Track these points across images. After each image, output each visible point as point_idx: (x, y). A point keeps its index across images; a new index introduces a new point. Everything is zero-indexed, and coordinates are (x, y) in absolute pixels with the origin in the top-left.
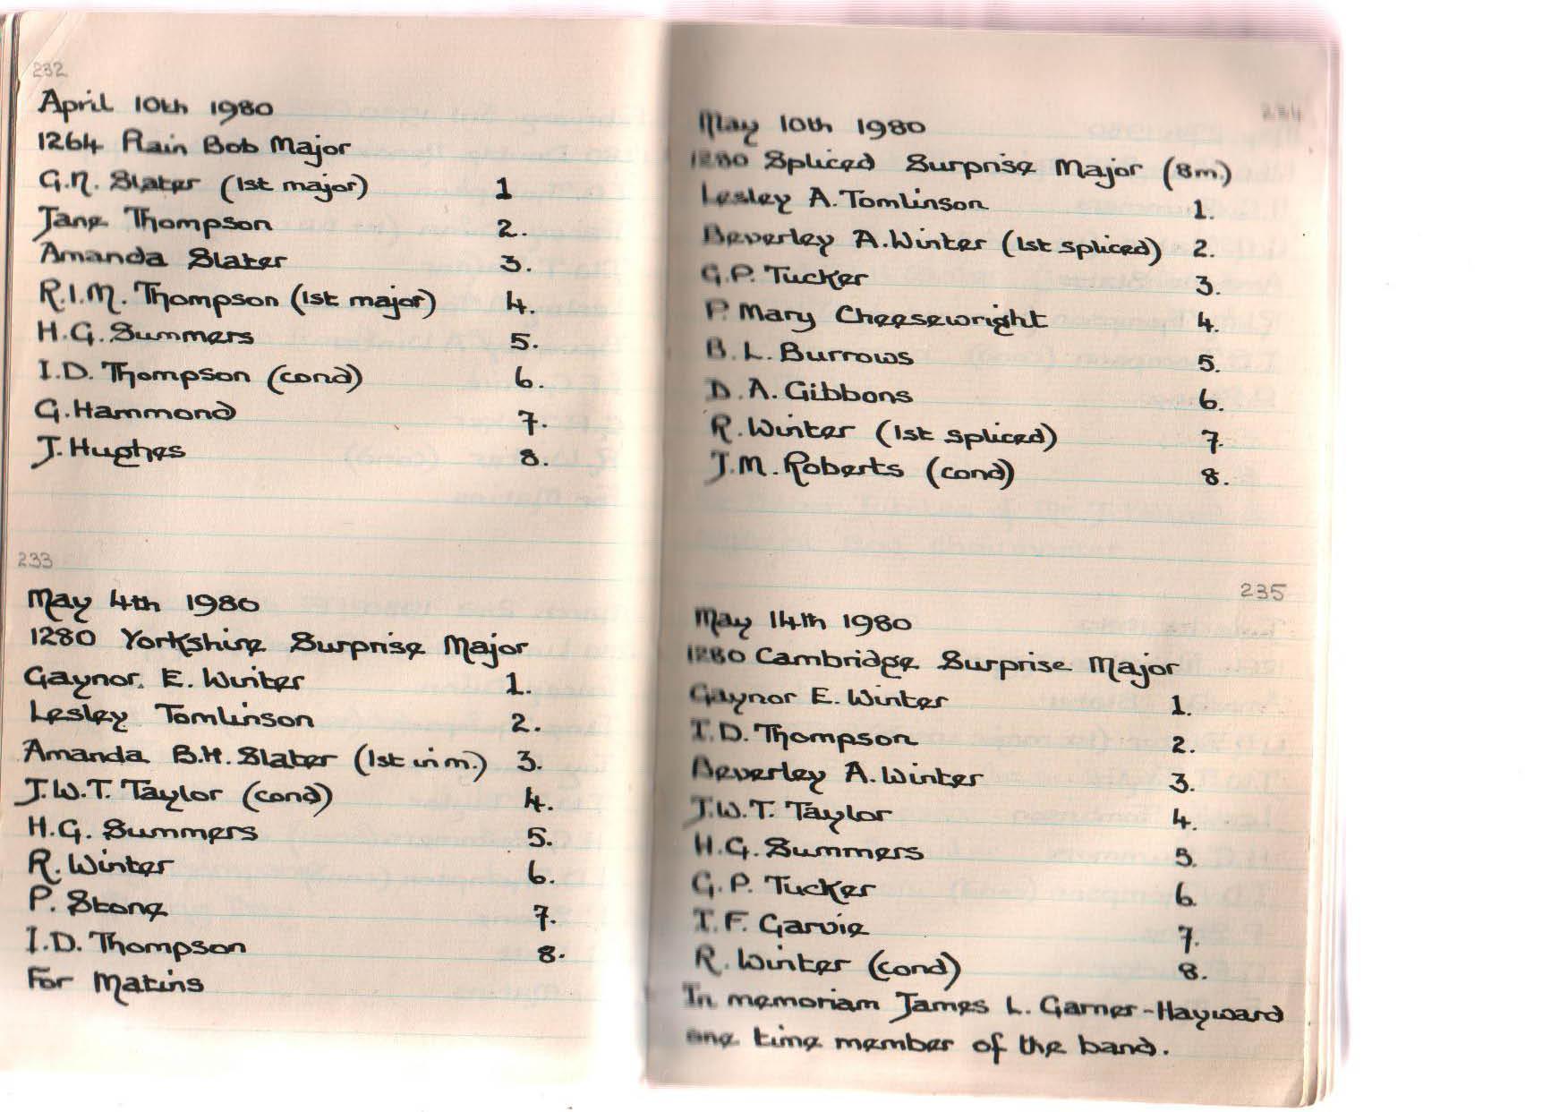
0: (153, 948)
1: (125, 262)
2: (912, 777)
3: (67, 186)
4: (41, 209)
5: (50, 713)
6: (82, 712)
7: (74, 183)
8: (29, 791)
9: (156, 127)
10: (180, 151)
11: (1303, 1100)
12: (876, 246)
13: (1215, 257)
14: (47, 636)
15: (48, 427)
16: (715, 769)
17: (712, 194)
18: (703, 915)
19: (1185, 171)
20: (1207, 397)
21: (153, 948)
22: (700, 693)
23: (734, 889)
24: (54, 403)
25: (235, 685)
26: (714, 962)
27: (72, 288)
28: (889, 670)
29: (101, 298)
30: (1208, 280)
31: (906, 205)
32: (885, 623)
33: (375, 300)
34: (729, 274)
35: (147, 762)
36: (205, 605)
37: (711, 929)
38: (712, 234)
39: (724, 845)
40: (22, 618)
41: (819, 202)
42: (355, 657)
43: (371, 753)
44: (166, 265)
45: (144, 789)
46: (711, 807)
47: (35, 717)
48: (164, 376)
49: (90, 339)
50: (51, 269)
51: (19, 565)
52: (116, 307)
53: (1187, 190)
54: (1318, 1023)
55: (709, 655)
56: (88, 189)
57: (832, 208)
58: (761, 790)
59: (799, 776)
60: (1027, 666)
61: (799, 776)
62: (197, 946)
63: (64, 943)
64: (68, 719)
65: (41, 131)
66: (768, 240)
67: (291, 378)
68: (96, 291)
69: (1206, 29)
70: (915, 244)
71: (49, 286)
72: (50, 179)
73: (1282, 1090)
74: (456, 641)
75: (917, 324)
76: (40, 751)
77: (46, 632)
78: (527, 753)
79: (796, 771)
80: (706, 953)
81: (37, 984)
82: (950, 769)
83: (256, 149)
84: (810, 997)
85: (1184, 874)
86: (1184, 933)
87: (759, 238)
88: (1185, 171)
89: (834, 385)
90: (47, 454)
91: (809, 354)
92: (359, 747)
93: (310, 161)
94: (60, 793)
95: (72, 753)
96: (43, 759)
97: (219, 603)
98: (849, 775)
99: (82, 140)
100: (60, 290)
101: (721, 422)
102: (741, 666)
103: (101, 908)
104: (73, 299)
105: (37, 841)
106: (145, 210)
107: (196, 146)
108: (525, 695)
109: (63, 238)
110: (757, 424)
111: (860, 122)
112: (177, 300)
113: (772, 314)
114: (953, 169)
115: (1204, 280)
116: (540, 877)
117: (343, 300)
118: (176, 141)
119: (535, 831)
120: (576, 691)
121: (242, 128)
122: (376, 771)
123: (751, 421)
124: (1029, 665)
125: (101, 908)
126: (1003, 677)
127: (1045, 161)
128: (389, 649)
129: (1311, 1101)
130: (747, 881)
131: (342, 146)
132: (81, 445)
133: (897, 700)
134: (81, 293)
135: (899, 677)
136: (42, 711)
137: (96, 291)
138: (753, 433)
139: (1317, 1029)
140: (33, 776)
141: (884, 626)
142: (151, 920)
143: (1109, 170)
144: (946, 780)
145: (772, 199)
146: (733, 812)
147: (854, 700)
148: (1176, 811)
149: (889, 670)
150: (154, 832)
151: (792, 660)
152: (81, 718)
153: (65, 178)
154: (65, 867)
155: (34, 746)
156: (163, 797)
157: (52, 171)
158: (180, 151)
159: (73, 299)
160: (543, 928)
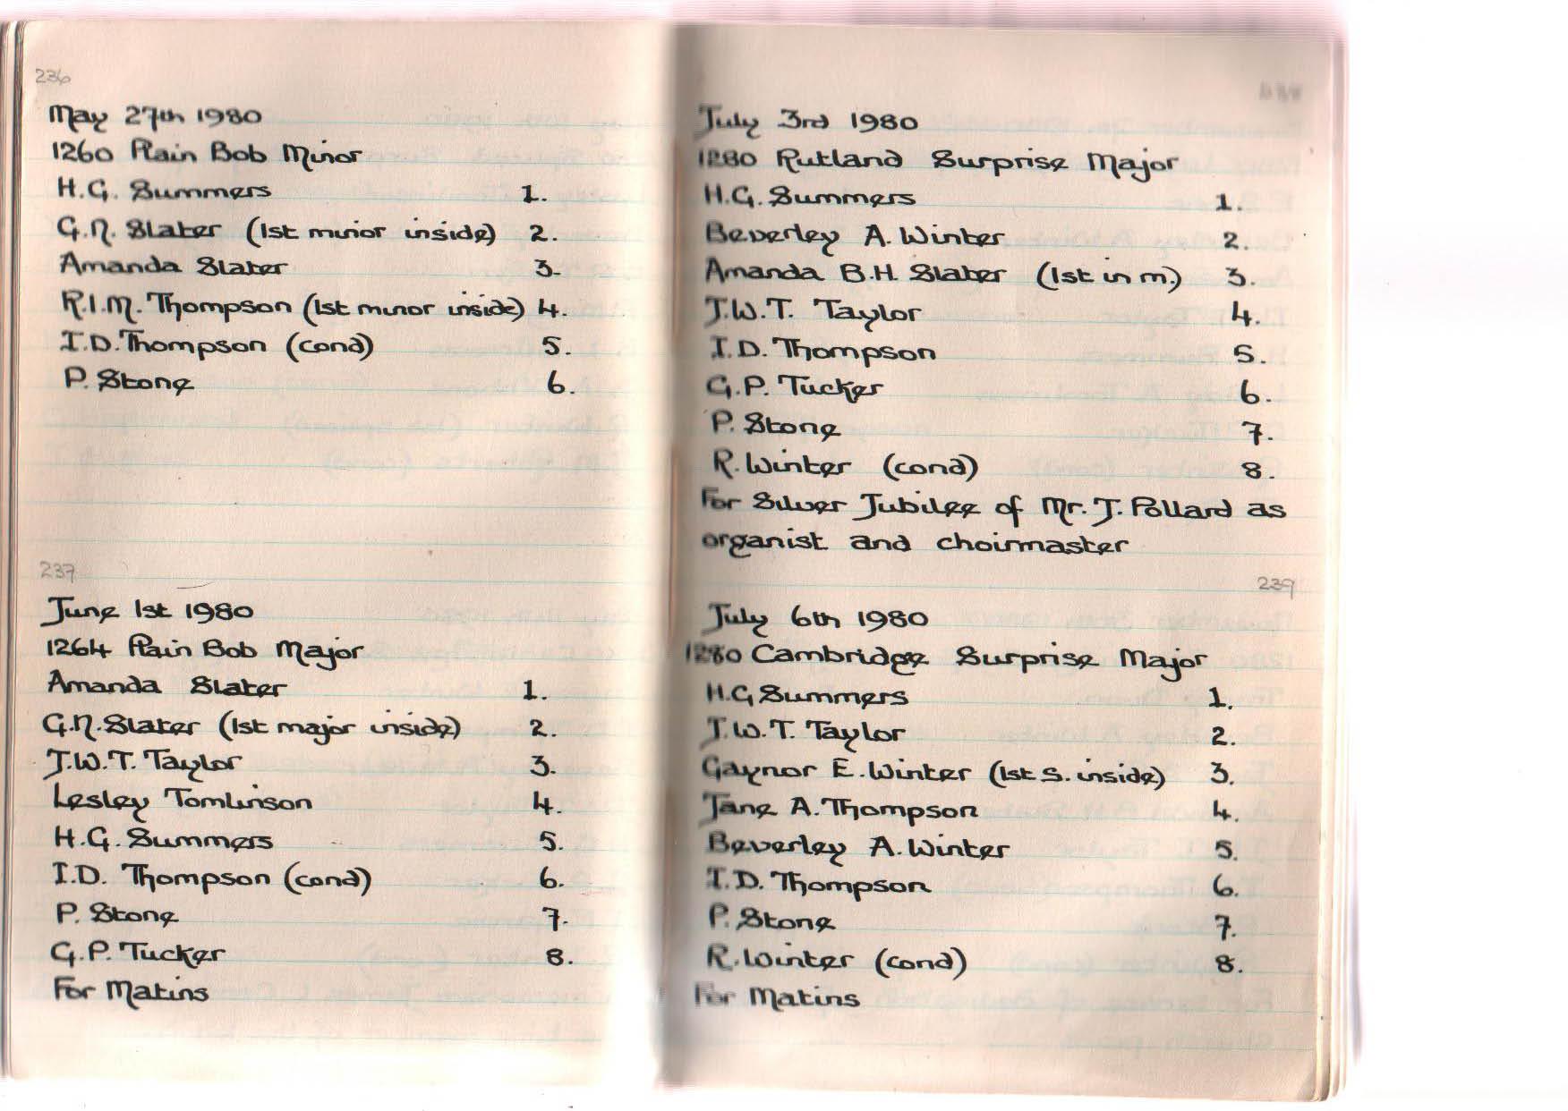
0: (176, 347)
1: (144, 271)
2: (934, 236)
3: (72, 729)
5: (70, 799)
6: (101, 799)
7: (94, 233)
10: (189, 158)
11: (1317, 1095)
14: (61, 648)
15: (55, 741)
16: (727, 233)
17: (63, 799)
18: (718, 609)
21: (176, 347)
22: (712, 767)
26: (725, 960)
27: (92, 298)
28: (900, 668)
32: (899, 619)
37: (723, 886)
38: (712, 159)
40: (31, 638)
41: (882, 852)
43: (263, 226)
46: (726, 308)
47: (57, 804)
50: (71, 280)
51: (43, 576)
52: (134, 316)
54: (1330, 1018)
56: (93, 733)
57: (896, 856)
58: (776, 287)
59: (819, 849)
60: (1050, 660)
61: (819, 849)
62: (220, 345)
63: (89, 876)
64: (88, 805)
67: (306, 881)
68: (116, 303)
69: (1211, 27)
71: (75, 296)
73: (1297, 1082)
74: (1132, 654)
76: (75, 263)
77: (67, 149)
78: (541, 757)
79: (816, 845)
80: (717, 951)
81: (63, 993)
83: (264, 158)
85: (1225, 867)
86: (1222, 921)
90: (56, 769)
91: (797, 197)
93: (322, 664)
94: (81, 764)
95: (92, 686)
96: (79, 272)
97: (216, 611)
101: (723, 456)
102: (753, 169)
103: (129, 384)
104: (93, 309)
105: (69, 359)
106: (794, 341)
107: (204, 153)
109: (72, 668)
111: (854, 116)
114: (1009, 661)
116: (558, 385)
117: (353, 308)
118: (185, 148)
119: (547, 835)
120: (587, 697)
121: (236, 137)
124: (1052, 659)
125: (129, 384)
126: (1025, 670)
128: (1061, 660)
129: (1324, 1097)
131: (354, 651)
132: (98, 648)
133: (919, 773)
134: (101, 303)
135: (912, 674)
136: (63, 799)
137: (116, 303)
139: (1329, 1024)
141: (899, 622)
142: (178, 394)
144: (974, 852)
145: (827, 848)
147: (916, 851)
149: (900, 668)
151: (765, 273)
152: (100, 805)
153: (69, 723)
156: (184, 766)
157: (68, 217)
158: (189, 158)
159: (93, 309)
160: (555, 928)
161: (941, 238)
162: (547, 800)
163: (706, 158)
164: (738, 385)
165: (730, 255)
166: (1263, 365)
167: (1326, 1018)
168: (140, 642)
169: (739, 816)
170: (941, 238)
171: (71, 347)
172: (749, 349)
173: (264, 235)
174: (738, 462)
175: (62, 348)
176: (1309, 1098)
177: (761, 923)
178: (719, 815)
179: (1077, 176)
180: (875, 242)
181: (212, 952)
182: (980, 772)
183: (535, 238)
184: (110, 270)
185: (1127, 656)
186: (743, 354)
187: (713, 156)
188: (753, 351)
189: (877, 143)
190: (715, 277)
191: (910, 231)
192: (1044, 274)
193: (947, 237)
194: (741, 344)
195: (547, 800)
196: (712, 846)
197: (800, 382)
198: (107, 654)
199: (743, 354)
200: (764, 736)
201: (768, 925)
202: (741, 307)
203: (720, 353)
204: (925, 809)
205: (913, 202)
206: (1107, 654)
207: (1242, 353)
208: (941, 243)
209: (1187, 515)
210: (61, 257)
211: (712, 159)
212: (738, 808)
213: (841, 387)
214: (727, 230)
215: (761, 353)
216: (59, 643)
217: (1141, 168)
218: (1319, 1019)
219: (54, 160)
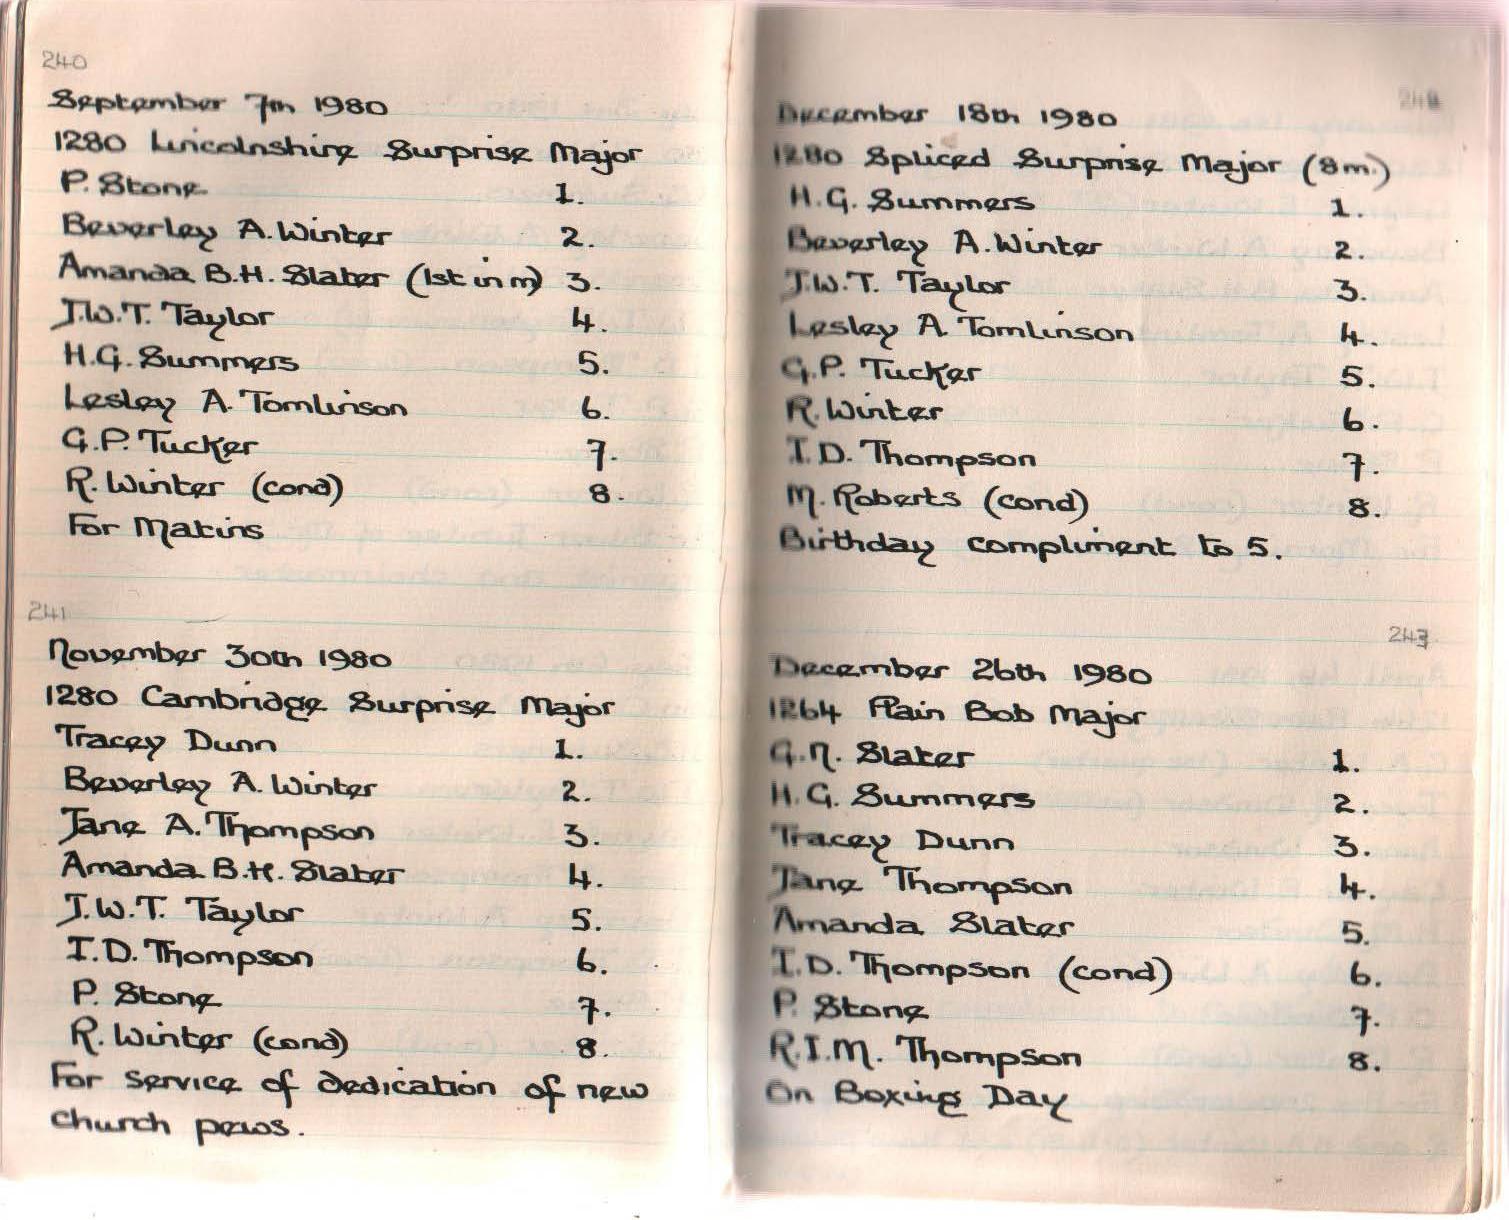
2: (1028, 244)
4: (58, 728)
7: (814, 755)
8: (62, 313)
9: (910, 692)
11: (1467, 1206)
12: (976, 250)
13: (1364, 217)
19: (1329, 166)
20: (1352, 418)
23: (824, 373)
24: (81, 432)
25: (143, 490)
29: (152, 533)
30: (1350, 285)
31: (1032, 334)
33: (108, 271)
34: (818, 371)
35: (193, 281)
36: (1092, 674)
37: (805, 460)
38: (789, 709)
39: (825, 197)
40: (35, 672)
42: (1089, 176)
43: (427, 272)
44: (65, 301)
45: (187, 312)
46: (807, 281)
47: (69, 405)
48: (203, 362)
49: (116, 364)
53: (1331, 186)
55: (75, 697)
58: (861, 261)
65: (49, 684)
66: (855, 246)
70: (1023, 247)
72: (74, 438)
73: (1446, 1193)
75: (1022, 208)
76: (75, 265)
81: (62, 1083)
82: (1072, 239)
83: (1031, 718)
84: (879, 1090)
87: (846, 243)
88: (1329, 166)
89: (813, 704)
92: (414, 266)
98: (960, 244)
99: (818, 708)
100: (96, 1031)
102: (840, 168)
108: (575, 760)
110: (836, 405)
112: (193, 958)
113: (836, 925)
115: (1345, 285)
122: (435, 291)
123: (829, 402)
127: (1168, 155)
129: (1475, 1208)
130: (839, 362)
136: (77, 397)
138: (831, 416)
140: (70, 296)
143: (1242, 164)
146: (831, 286)
148: (1345, 326)
150: (192, 360)
154: (103, 484)
155: (69, 259)
157: (76, 429)
161: (1036, 247)
162: (587, 317)
163: (778, 710)
164: (814, 367)
165: (803, 904)
166: (1374, 347)
167: (1478, 1120)
168: (887, 703)
169: (816, 893)
170: (1036, 247)
171: (78, 956)
172: (832, 454)
173: (429, 282)
174: (818, 409)
175: (69, 957)
176: (1458, 1211)
177: (838, 1013)
178: (789, 888)
179: (1172, 181)
180: (967, 250)
181: (152, 484)
182: (218, 653)
183: (567, 243)
184: (112, 276)
185: (558, 150)
186: (824, 459)
187: (787, 705)
188: (836, 456)
189: (972, 138)
190: (785, 926)
191: (1006, 238)
192: (418, 272)
193: (1042, 246)
194: (823, 447)
195: (587, 317)
196: (791, 243)
197: (883, 366)
198: (1359, 895)
199: (824, 459)
200: (850, 460)
201: (848, 1014)
202: (823, 279)
203: (799, 457)
204: (1020, 1055)
205: (1031, 207)
206: (1170, 160)
207: (1352, 931)
208: (1035, 252)
209: (998, 931)
210: (61, 256)
211: (789, 709)
212: (815, 883)
213: (933, 372)
214: (89, 777)
215: (835, 970)
216: (982, 663)
217: (1238, 171)
218: (1469, 1122)
219: (55, 151)
